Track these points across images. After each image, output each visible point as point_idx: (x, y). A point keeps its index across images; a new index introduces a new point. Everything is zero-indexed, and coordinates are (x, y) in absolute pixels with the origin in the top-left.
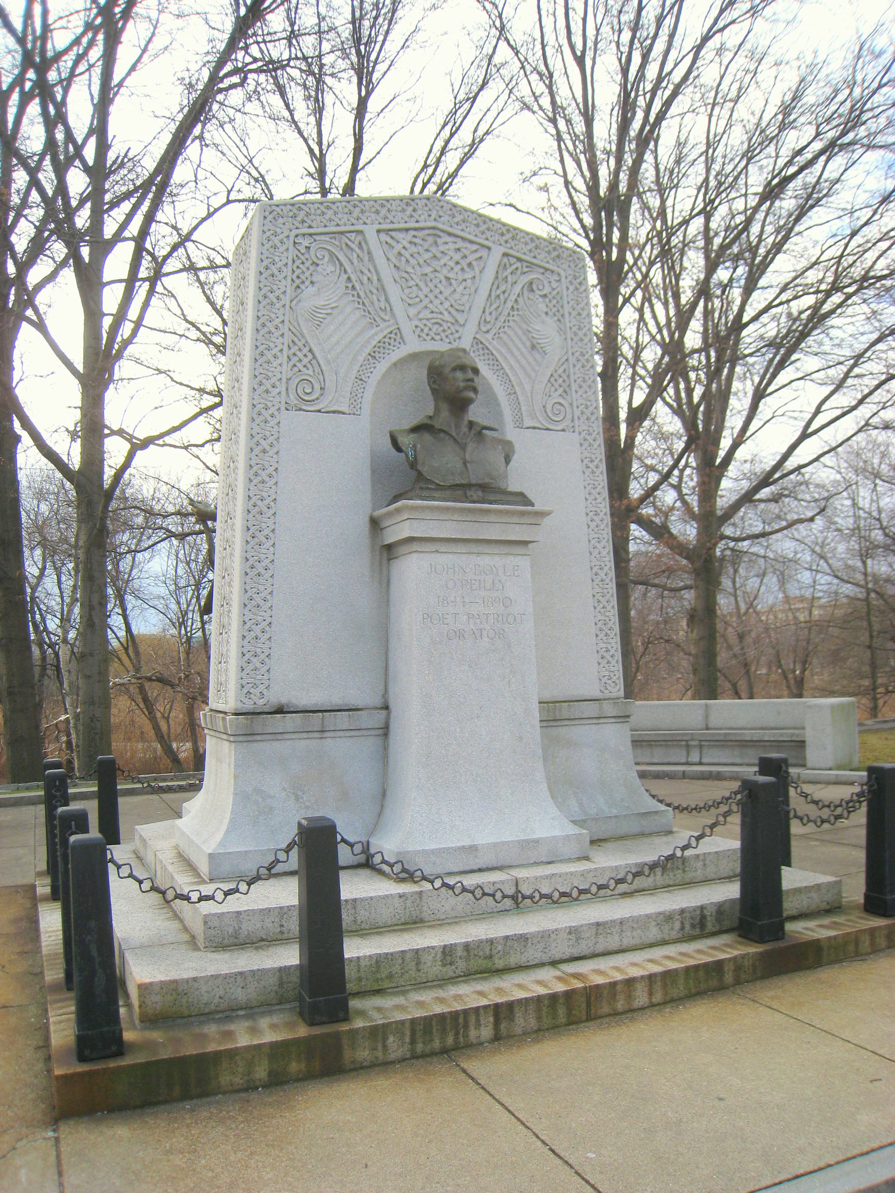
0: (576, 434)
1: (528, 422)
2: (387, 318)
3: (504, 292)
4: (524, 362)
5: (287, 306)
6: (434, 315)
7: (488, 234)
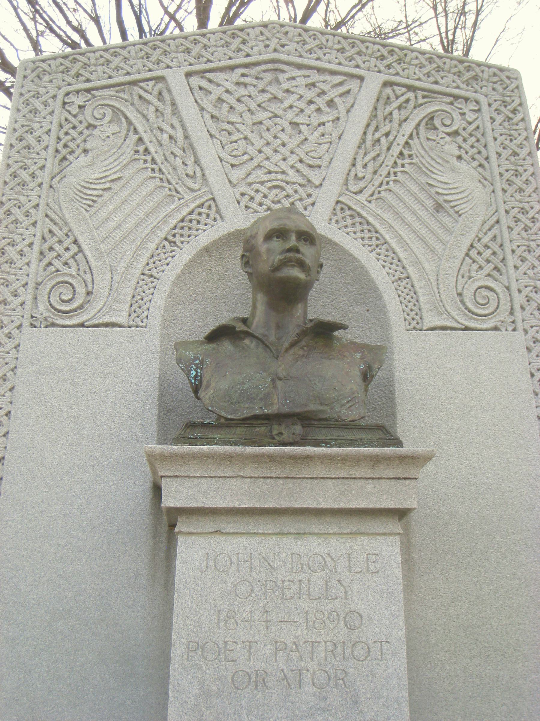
0: (520, 333)
1: (431, 320)
2: (196, 186)
3: (387, 135)
4: (423, 232)
5: (45, 186)
6: (272, 176)
7: (359, 60)
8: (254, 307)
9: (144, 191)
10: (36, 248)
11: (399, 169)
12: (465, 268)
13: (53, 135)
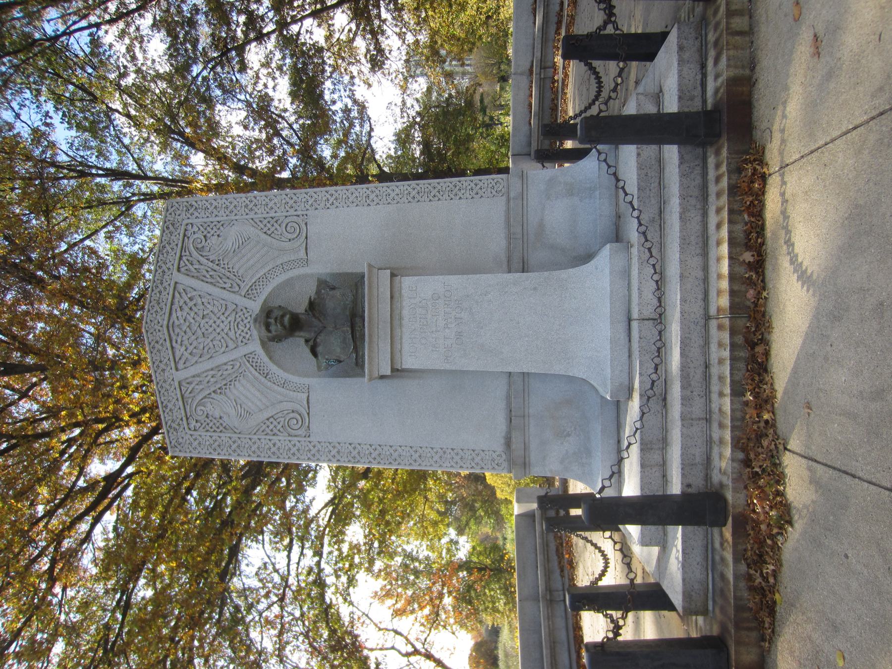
2: (238, 364)
3: (207, 271)
7: (165, 284)
8: (301, 337)
9: (241, 388)
10: (271, 438)
11: (226, 266)
12: (277, 237)
13: (213, 434)
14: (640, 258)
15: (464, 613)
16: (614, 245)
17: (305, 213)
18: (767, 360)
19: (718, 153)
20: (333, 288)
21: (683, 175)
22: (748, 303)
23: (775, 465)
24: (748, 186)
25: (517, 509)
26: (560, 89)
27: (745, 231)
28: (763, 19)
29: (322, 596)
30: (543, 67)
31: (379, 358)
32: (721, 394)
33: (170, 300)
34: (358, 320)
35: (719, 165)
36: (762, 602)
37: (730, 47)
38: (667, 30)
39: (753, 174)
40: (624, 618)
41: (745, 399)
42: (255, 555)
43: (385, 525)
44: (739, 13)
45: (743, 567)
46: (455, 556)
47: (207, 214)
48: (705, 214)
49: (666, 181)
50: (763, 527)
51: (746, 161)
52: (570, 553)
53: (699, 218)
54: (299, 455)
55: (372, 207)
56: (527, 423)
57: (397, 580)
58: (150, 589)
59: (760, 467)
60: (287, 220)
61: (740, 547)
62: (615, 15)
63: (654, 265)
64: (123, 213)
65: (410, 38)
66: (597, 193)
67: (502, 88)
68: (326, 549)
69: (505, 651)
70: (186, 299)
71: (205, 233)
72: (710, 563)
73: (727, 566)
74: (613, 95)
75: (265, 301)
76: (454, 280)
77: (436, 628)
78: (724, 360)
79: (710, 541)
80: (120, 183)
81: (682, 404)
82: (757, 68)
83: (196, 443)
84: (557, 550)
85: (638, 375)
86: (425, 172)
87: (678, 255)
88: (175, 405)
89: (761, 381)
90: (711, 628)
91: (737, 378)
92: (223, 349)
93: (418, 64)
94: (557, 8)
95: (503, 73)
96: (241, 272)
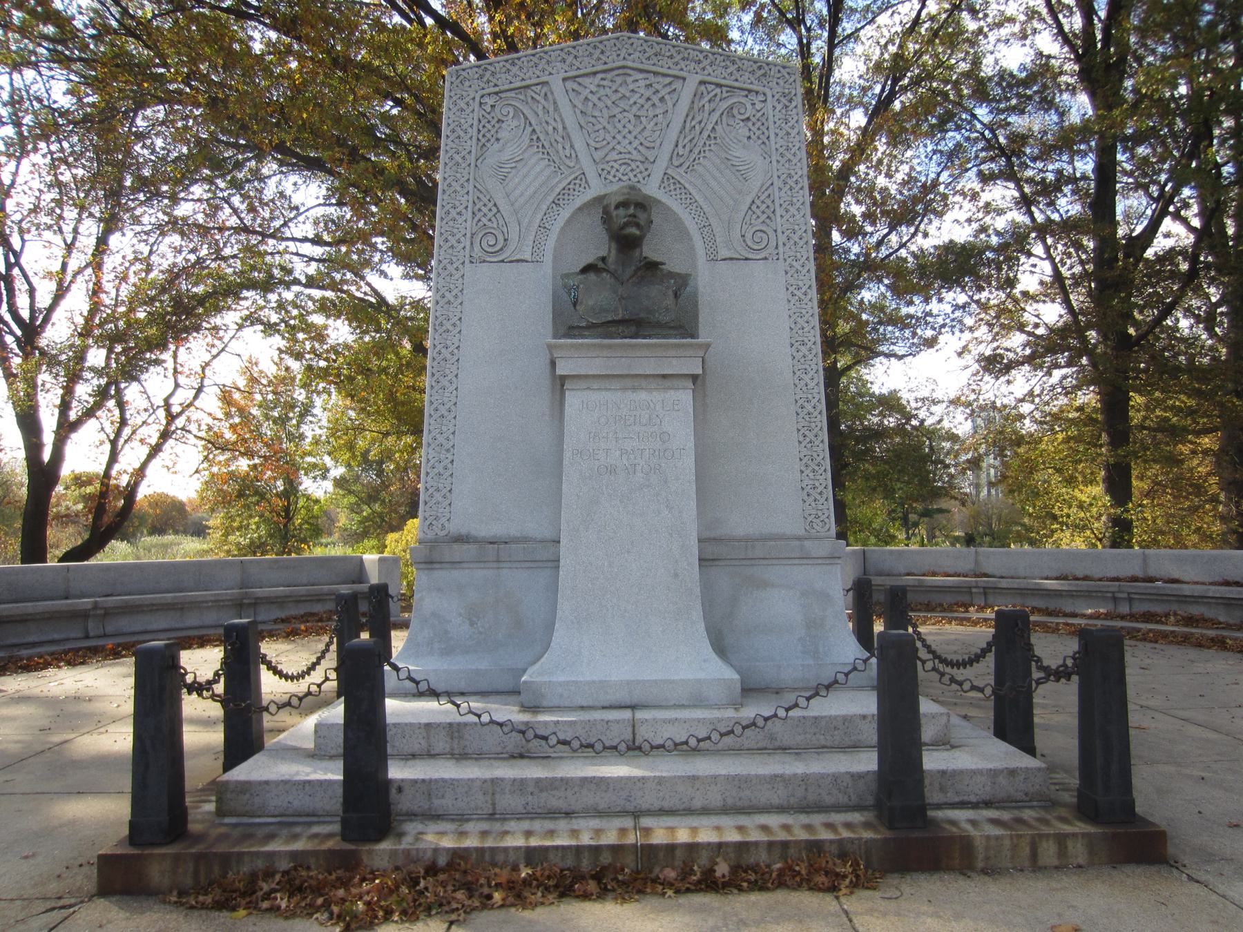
2: (572, 164)
7: (682, 64)
9: (538, 169)
11: (707, 148)
12: (747, 218)
14: (720, 720)
15: (225, 487)
16: (739, 685)
17: (781, 256)
18: (577, 897)
19: (867, 825)
20: (676, 296)
21: (836, 778)
22: (657, 870)
23: (428, 909)
24: (821, 869)
25: (370, 557)
26: (956, 615)
27: (758, 865)
28: (1054, 885)
29: (253, 285)
30: (986, 591)
31: (580, 359)
32: (528, 834)
33: (661, 70)
34: (633, 329)
35: (851, 827)
36: (234, 891)
37: (1015, 841)
38: (1038, 754)
39: (837, 875)
40: (214, 697)
41: (522, 866)
42: (309, 194)
43: (352, 375)
44: (1062, 852)
45: (284, 865)
46: (306, 474)
47: (779, 123)
48: (781, 809)
49: (827, 756)
50: (341, 892)
51: (856, 864)
52: (308, 632)
53: (776, 801)
54: (445, 248)
55: (788, 349)
56: (487, 565)
57: (274, 393)
58: (262, 47)
59: (426, 889)
60: (771, 232)
61: (312, 861)
62: (1058, 680)
63: (709, 738)
64: (782, 14)
65: (1026, 408)
66: (811, 662)
67: (957, 539)
68: (317, 293)
69: (172, 544)
70: (663, 93)
71: (754, 120)
72: (291, 819)
73: (287, 842)
74: (946, 679)
75: (659, 202)
76: (688, 462)
77: (205, 448)
78: (577, 838)
79: (322, 819)
80: (825, 12)
81: (515, 780)
82: (987, 878)
83: (462, 104)
84: (312, 614)
85: (555, 719)
86: (841, 433)
87: (723, 772)
88: (516, 76)
89: (547, 889)
90: (198, 821)
91: (551, 856)
92: (593, 144)
93: (989, 421)
94: (1068, 609)
95: (978, 540)
96: (699, 169)
